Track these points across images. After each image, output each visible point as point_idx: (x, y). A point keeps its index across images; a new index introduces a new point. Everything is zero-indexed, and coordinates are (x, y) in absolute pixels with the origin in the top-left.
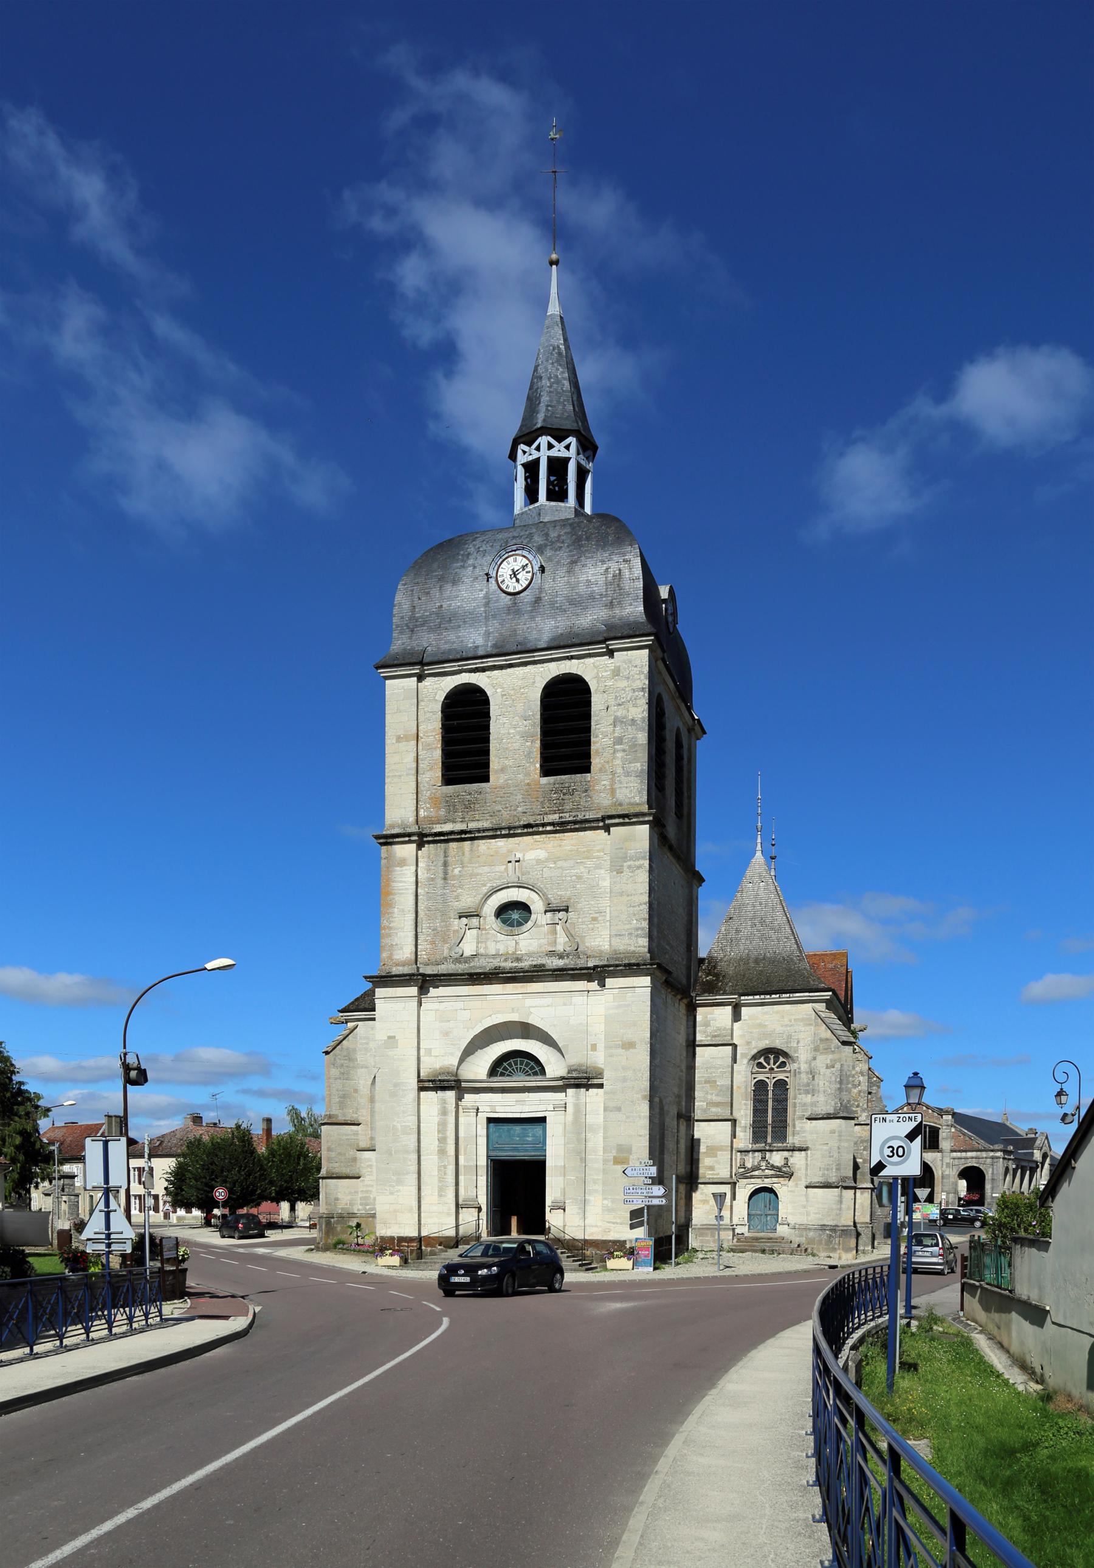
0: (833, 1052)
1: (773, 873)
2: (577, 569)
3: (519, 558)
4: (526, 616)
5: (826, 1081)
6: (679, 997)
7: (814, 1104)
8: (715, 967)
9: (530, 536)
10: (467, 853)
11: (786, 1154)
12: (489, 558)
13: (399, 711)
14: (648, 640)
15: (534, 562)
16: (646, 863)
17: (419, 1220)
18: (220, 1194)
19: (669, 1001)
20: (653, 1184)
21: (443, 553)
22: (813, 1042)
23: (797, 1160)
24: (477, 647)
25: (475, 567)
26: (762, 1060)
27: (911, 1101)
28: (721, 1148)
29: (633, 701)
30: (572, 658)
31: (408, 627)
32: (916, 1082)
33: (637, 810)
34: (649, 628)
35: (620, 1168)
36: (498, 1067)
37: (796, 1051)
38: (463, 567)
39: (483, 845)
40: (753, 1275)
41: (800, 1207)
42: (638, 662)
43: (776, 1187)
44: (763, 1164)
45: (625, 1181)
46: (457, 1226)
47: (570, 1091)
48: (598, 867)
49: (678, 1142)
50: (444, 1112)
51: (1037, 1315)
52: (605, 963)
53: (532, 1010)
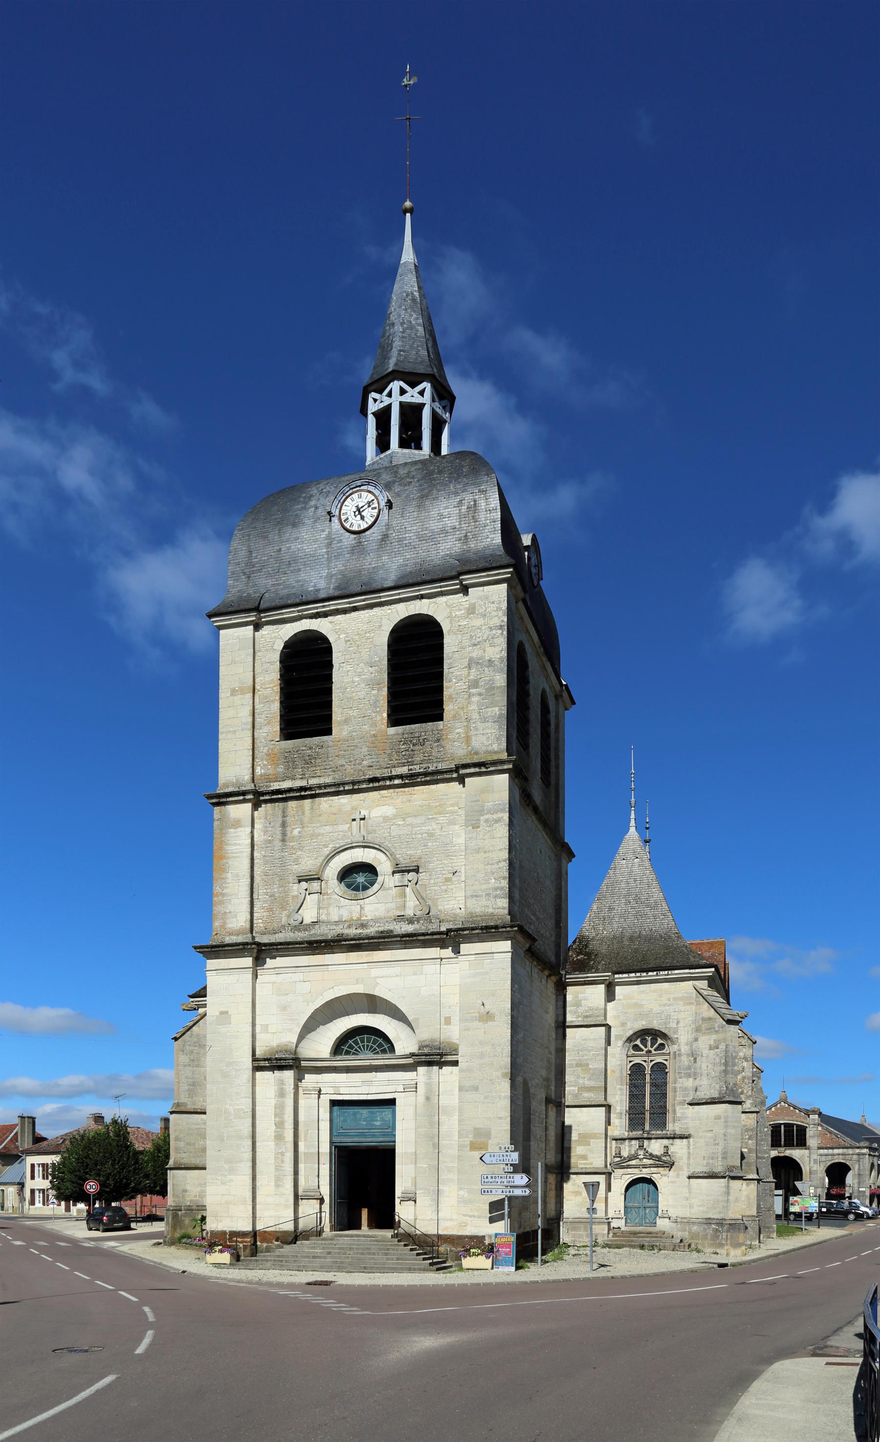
0: (717, 1032)
3: (364, 494)
6: (547, 973)
8: (587, 946)
11: (666, 1142)
13: (233, 662)
15: (380, 498)
16: (506, 816)
18: (91, 1187)
19: (535, 975)
20: (515, 1172)
23: (678, 1148)
24: (318, 590)
25: (317, 508)
26: (638, 1042)
28: (594, 1136)
29: (491, 641)
30: (422, 597)
31: (244, 574)
33: (495, 757)
34: (507, 560)
35: (477, 1154)
36: (341, 1045)
38: (305, 508)
39: (324, 803)
41: (681, 1199)
42: (495, 598)
43: (655, 1178)
44: (641, 1152)
45: (483, 1169)
46: (296, 1220)
48: (452, 823)
49: (546, 1129)
50: (281, 1094)
53: (378, 980)
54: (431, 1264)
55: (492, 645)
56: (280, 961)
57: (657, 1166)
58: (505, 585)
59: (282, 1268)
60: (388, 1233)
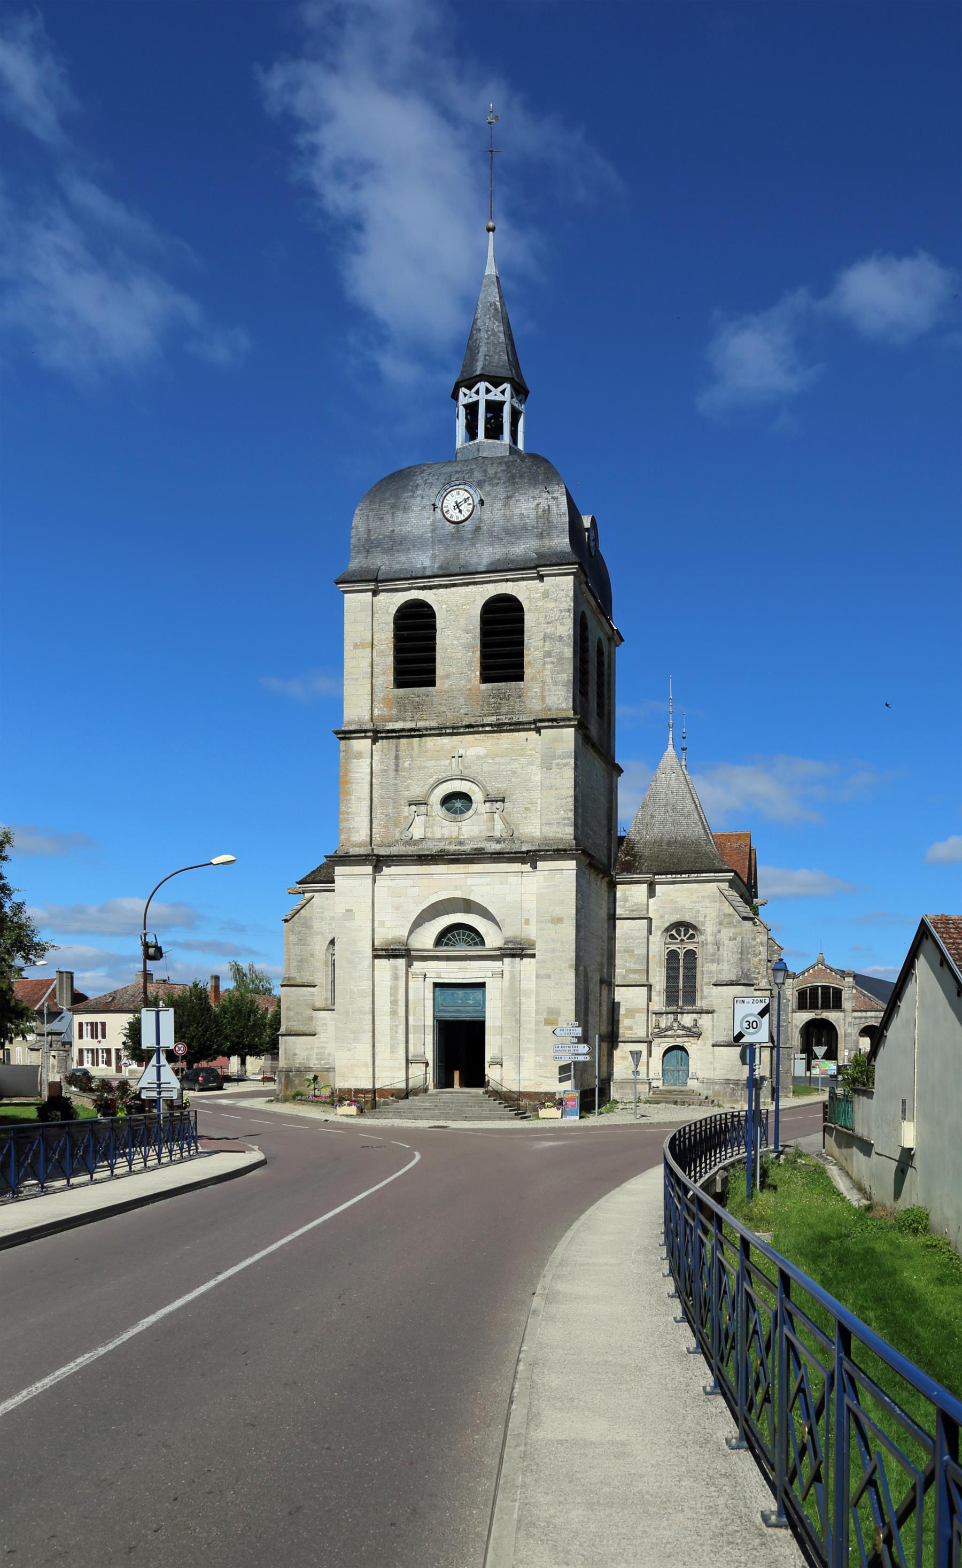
1: (683, 763)
2: (512, 502)
3: (462, 492)
4: (468, 543)
5: (729, 952)
6: (601, 876)
7: (719, 972)
8: (632, 848)
9: (471, 472)
10: (416, 748)
11: (695, 1016)
12: (436, 490)
13: (356, 621)
14: (574, 568)
15: (475, 496)
16: (572, 761)
17: (374, 1074)
20: (578, 1043)
21: (395, 484)
22: (718, 916)
24: (425, 568)
25: (423, 498)
26: (674, 932)
27: (777, 981)
28: (638, 1011)
29: (560, 620)
30: (507, 580)
31: (364, 548)
32: (782, 966)
34: (574, 558)
35: (550, 1029)
36: (441, 939)
37: (703, 925)
38: (412, 497)
39: (430, 742)
40: (665, 1123)
42: (564, 587)
43: (686, 1045)
44: (676, 1025)
46: (407, 1080)
47: (506, 960)
48: (531, 763)
49: (600, 1005)
50: (395, 977)
51: (866, 1148)
52: (537, 848)
54: (516, 1114)
55: (562, 624)
56: (394, 870)
57: (688, 1036)
58: (572, 577)
59: (401, 1117)
60: (480, 1091)
